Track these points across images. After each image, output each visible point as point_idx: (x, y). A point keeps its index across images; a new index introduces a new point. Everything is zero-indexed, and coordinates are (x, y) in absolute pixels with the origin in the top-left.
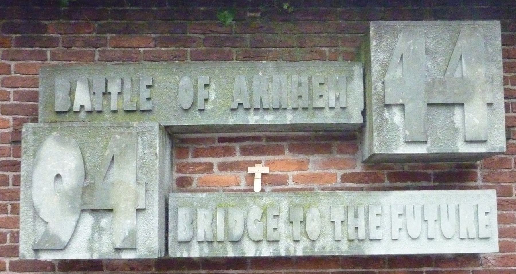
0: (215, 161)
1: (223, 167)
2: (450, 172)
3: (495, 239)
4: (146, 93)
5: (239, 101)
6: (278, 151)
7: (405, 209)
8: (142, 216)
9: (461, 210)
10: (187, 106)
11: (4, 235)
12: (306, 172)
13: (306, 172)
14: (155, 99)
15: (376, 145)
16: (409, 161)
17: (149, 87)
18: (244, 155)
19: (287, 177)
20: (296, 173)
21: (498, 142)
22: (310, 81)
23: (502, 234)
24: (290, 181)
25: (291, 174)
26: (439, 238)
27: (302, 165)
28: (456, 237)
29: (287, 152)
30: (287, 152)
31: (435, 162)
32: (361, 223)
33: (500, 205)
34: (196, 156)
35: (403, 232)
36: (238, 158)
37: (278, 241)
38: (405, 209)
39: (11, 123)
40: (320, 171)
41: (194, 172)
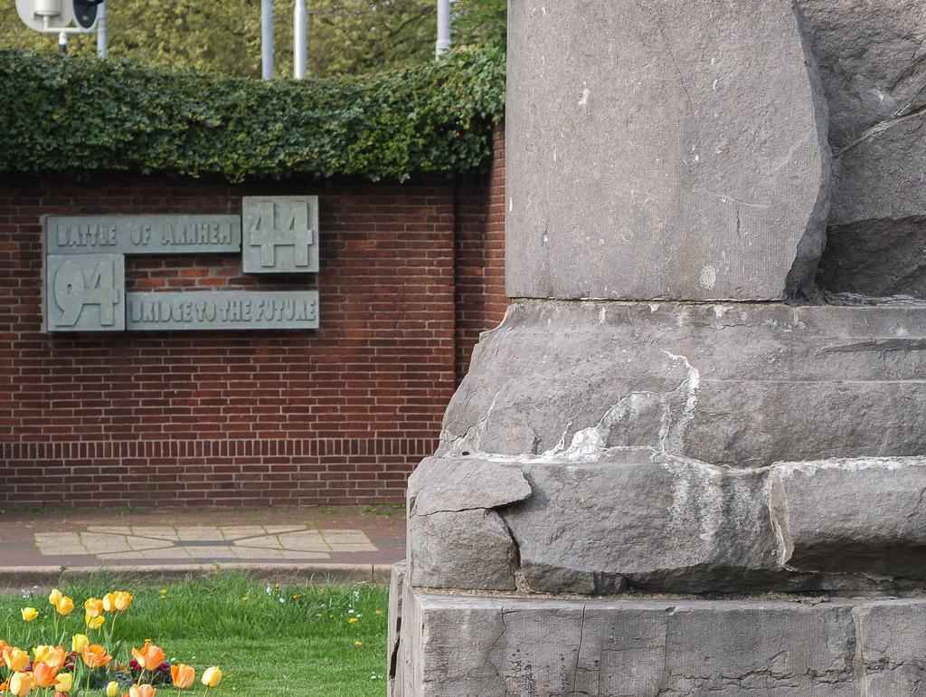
0: (149, 270)
1: (154, 274)
5: (167, 239)
6: (190, 265)
7: (263, 303)
8: (116, 307)
12: (206, 278)
13: (206, 278)
14: (118, 238)
15: (249, 266)
17: (114, 231)
19: (194, 281)
20: (200, 278)
22: (209, 227)
23: (322, 317)
24: (197, 283)
25: (197, 279)
27: (204, 273)
29: (194, 265)
30: (194, 265)
33: (321, 299)
34: (137, 267)
36: (163, 268)
37: (293, 245)
38: (263, 303)
39: (18, 246)
40: (216, 277)
41: (136, 278)
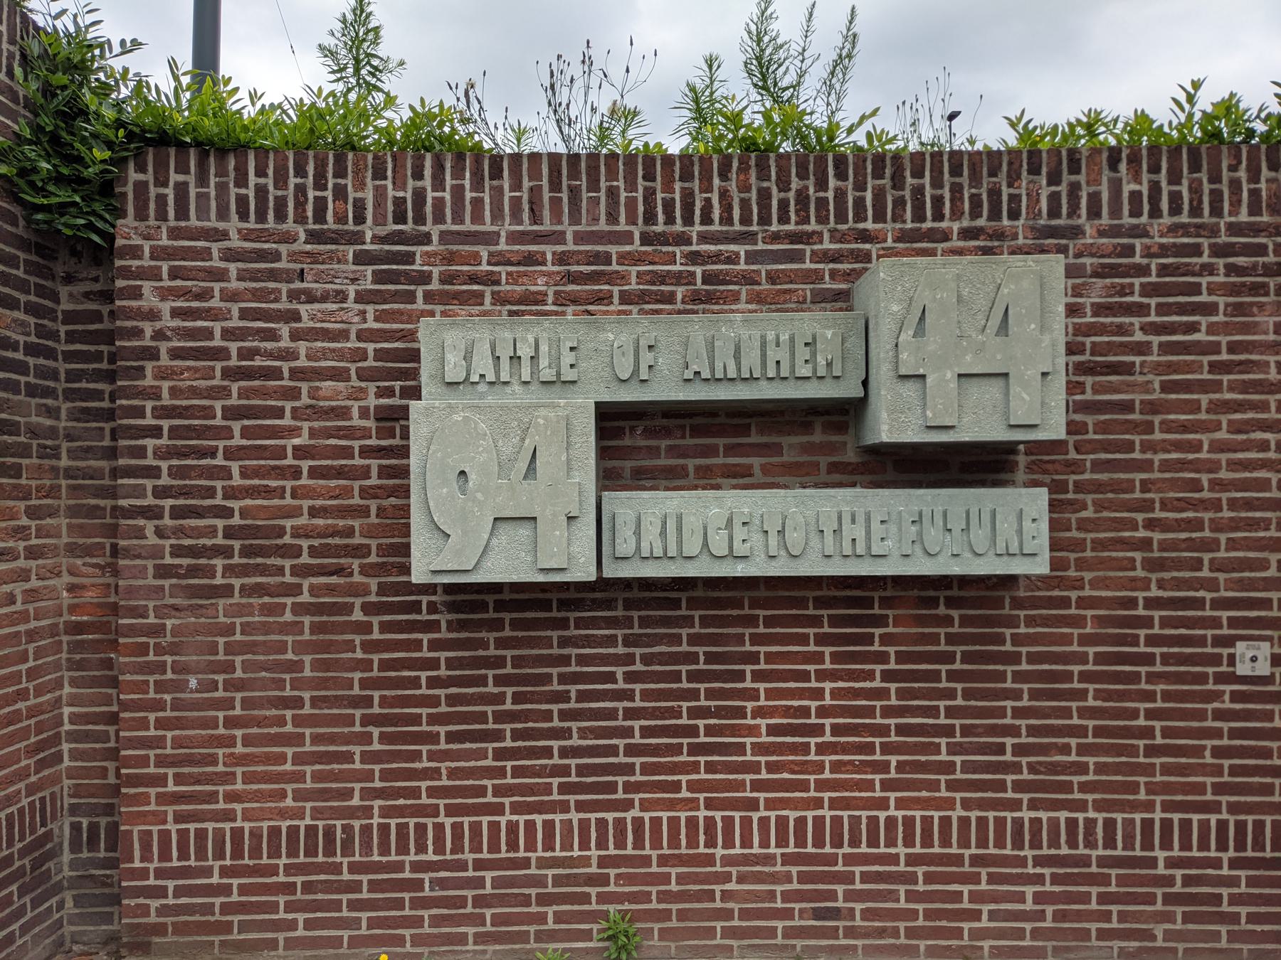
2: (978, 465)
3: (1046, 555)
4: (568, 358)
9: (998, 517)
10: (625, 376)
11: (1279, 410)
16: (827, 413)
17: (572, 349)
18: (647, 438)
21: (1055, 429)
26: (968, 555)
28: (991, 553)
31: (332, 536)
32: (860, 533)
35: (918, 548)
